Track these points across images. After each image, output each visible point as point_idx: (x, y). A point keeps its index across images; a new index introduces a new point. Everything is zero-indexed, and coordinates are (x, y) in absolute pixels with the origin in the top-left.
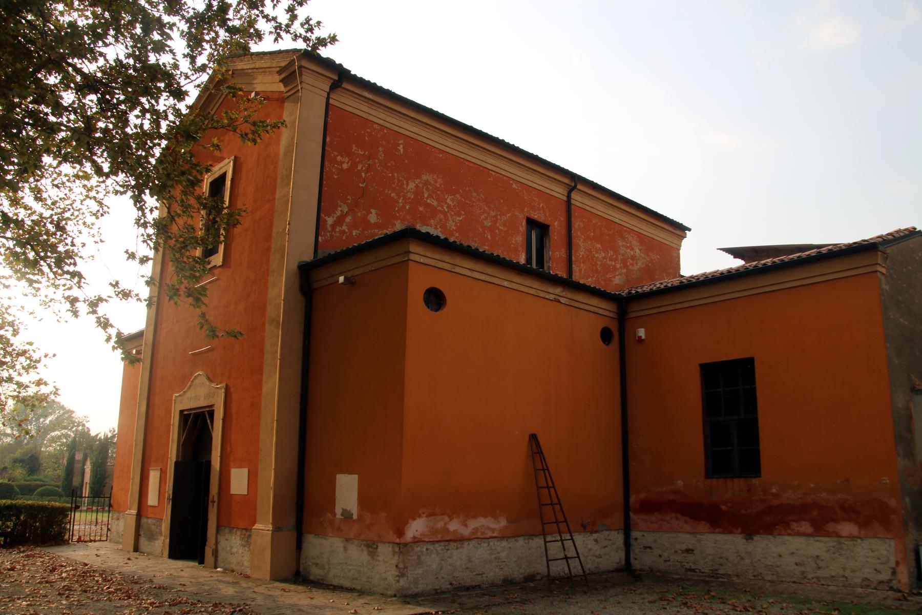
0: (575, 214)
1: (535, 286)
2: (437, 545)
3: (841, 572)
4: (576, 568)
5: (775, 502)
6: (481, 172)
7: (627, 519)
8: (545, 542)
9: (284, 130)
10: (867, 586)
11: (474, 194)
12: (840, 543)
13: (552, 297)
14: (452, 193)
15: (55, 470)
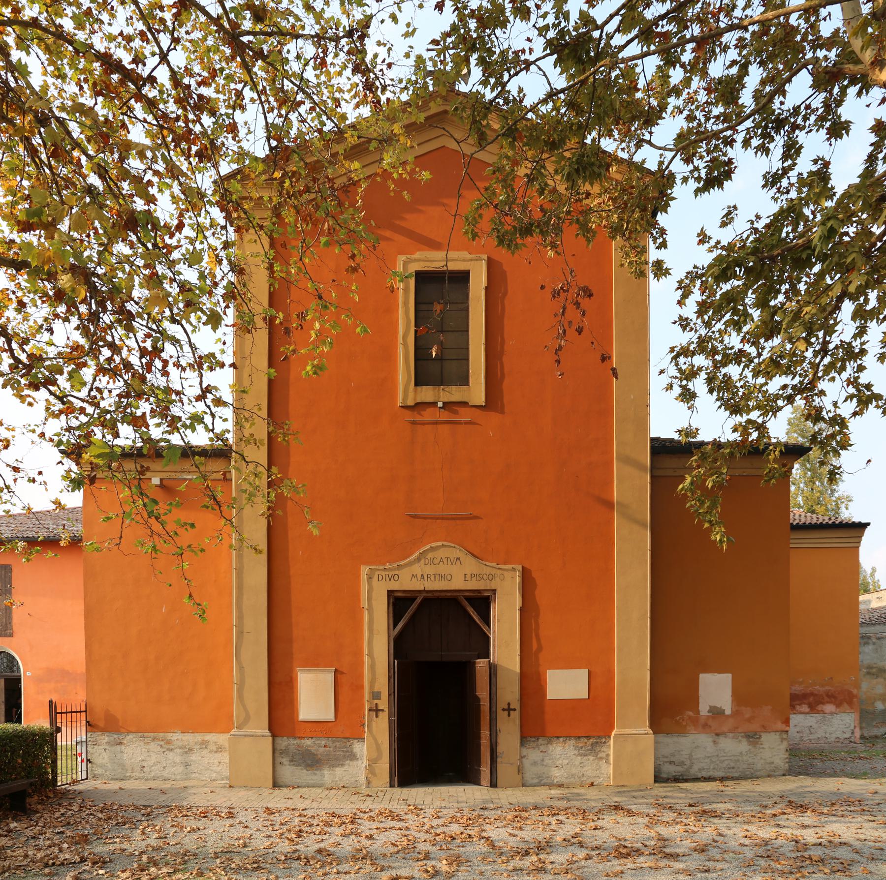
3: (824, 735)
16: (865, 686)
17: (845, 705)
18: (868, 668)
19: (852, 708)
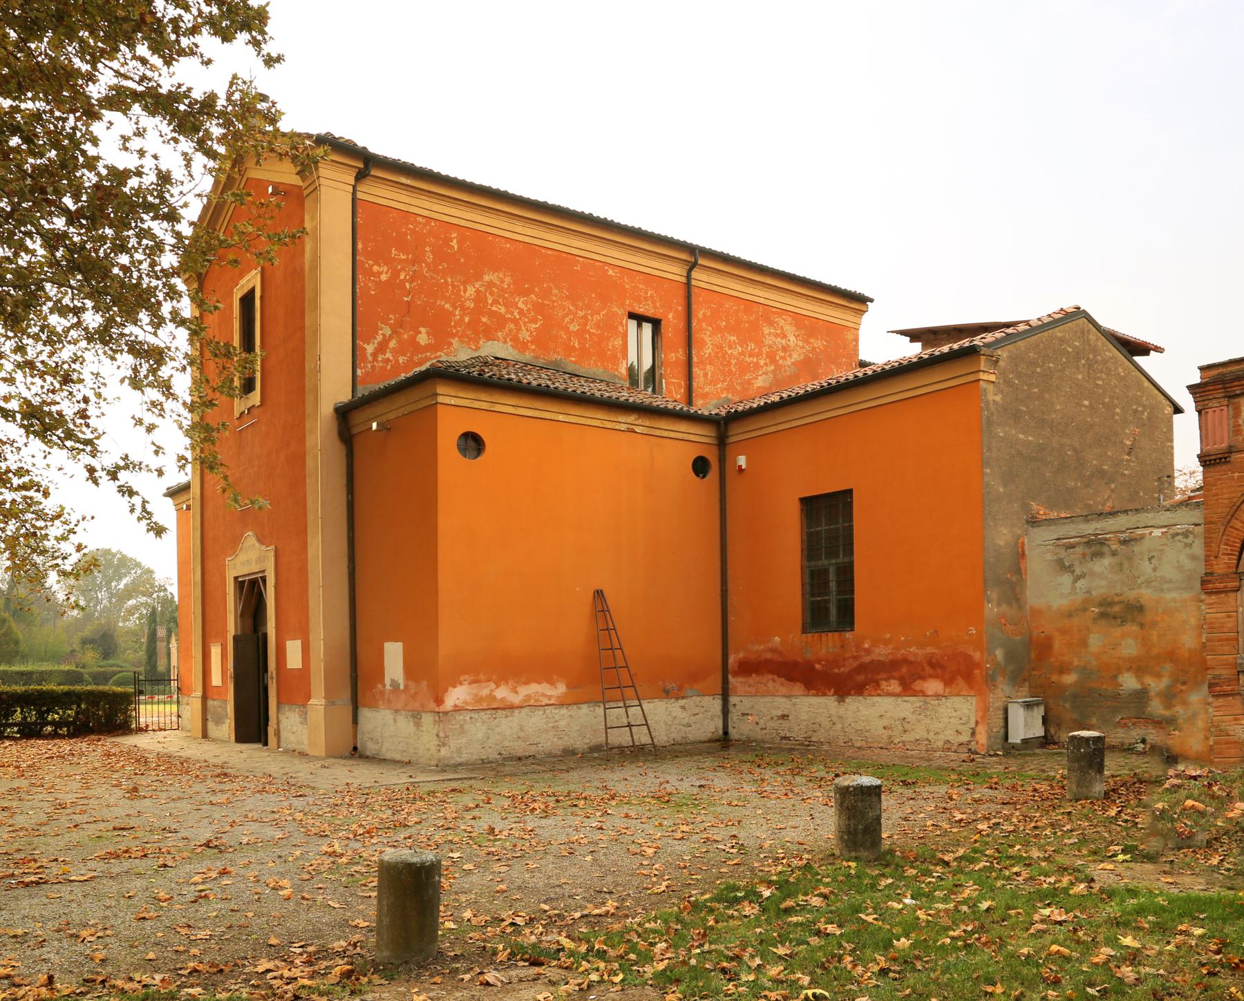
0: (697, 298)
1: (599, 416)
2: (482, 714)
3: (925, 735)
4: (642, 737)
5: (867, 659)
6: (564, 259)
7: (725, 681)
8: (605, 709)
9: (307, 239)
10: (949, 749)
11: (555, 291)
12: (926, 703)
13: (624, 427)
14: (525, 293)
15: (135, 651)
16: (1095, 641)
17: (960, 681)
18: (1101, 605)
19: (971, 687)
